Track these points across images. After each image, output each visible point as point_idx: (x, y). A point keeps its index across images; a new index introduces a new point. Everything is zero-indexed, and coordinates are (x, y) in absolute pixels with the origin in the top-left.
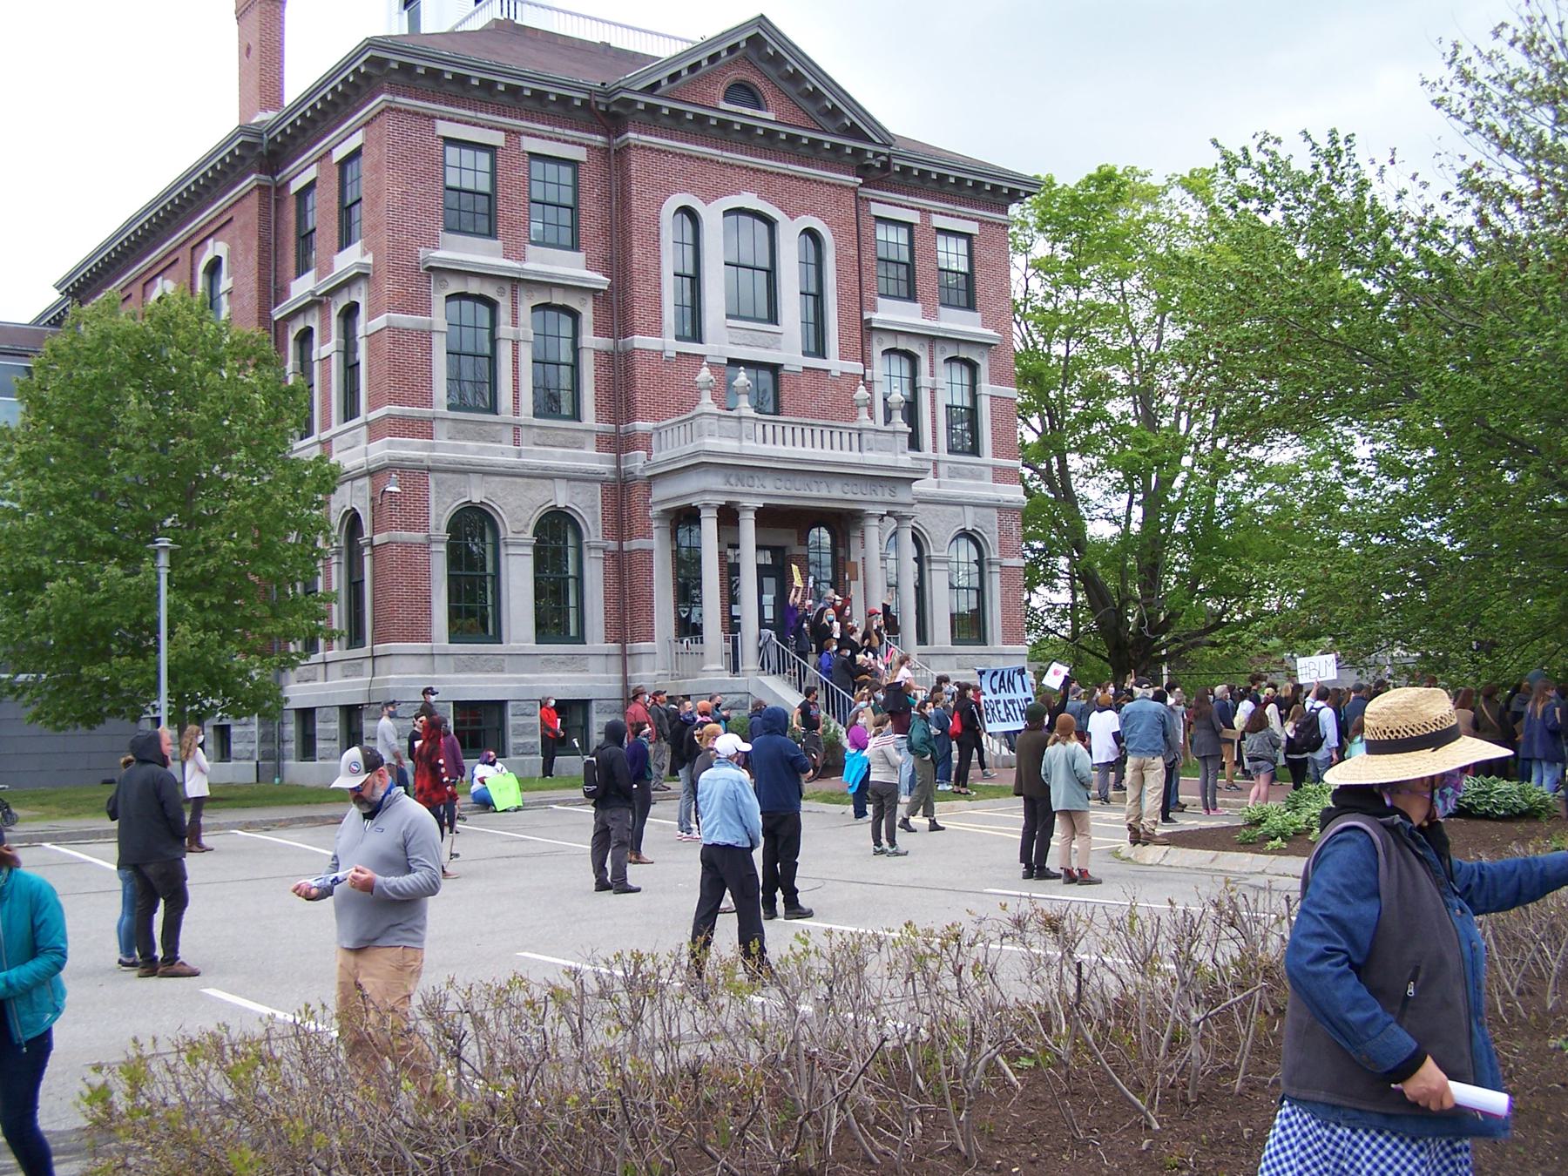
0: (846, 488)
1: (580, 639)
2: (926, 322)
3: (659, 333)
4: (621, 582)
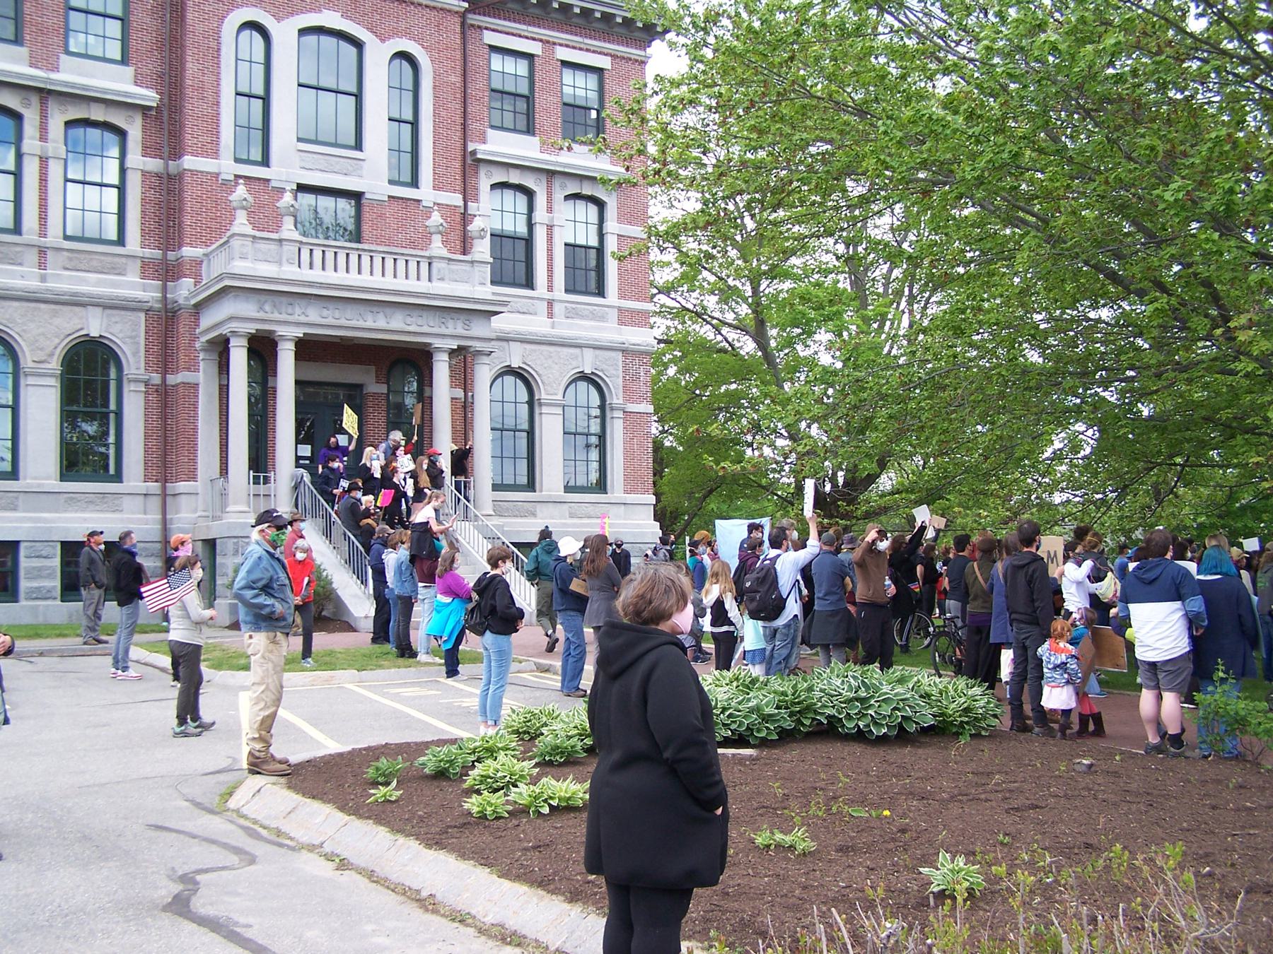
0: (409, 320)
1: (118, 478)
2: (545, 157)
3: (215, 154)
4: (164, 417)
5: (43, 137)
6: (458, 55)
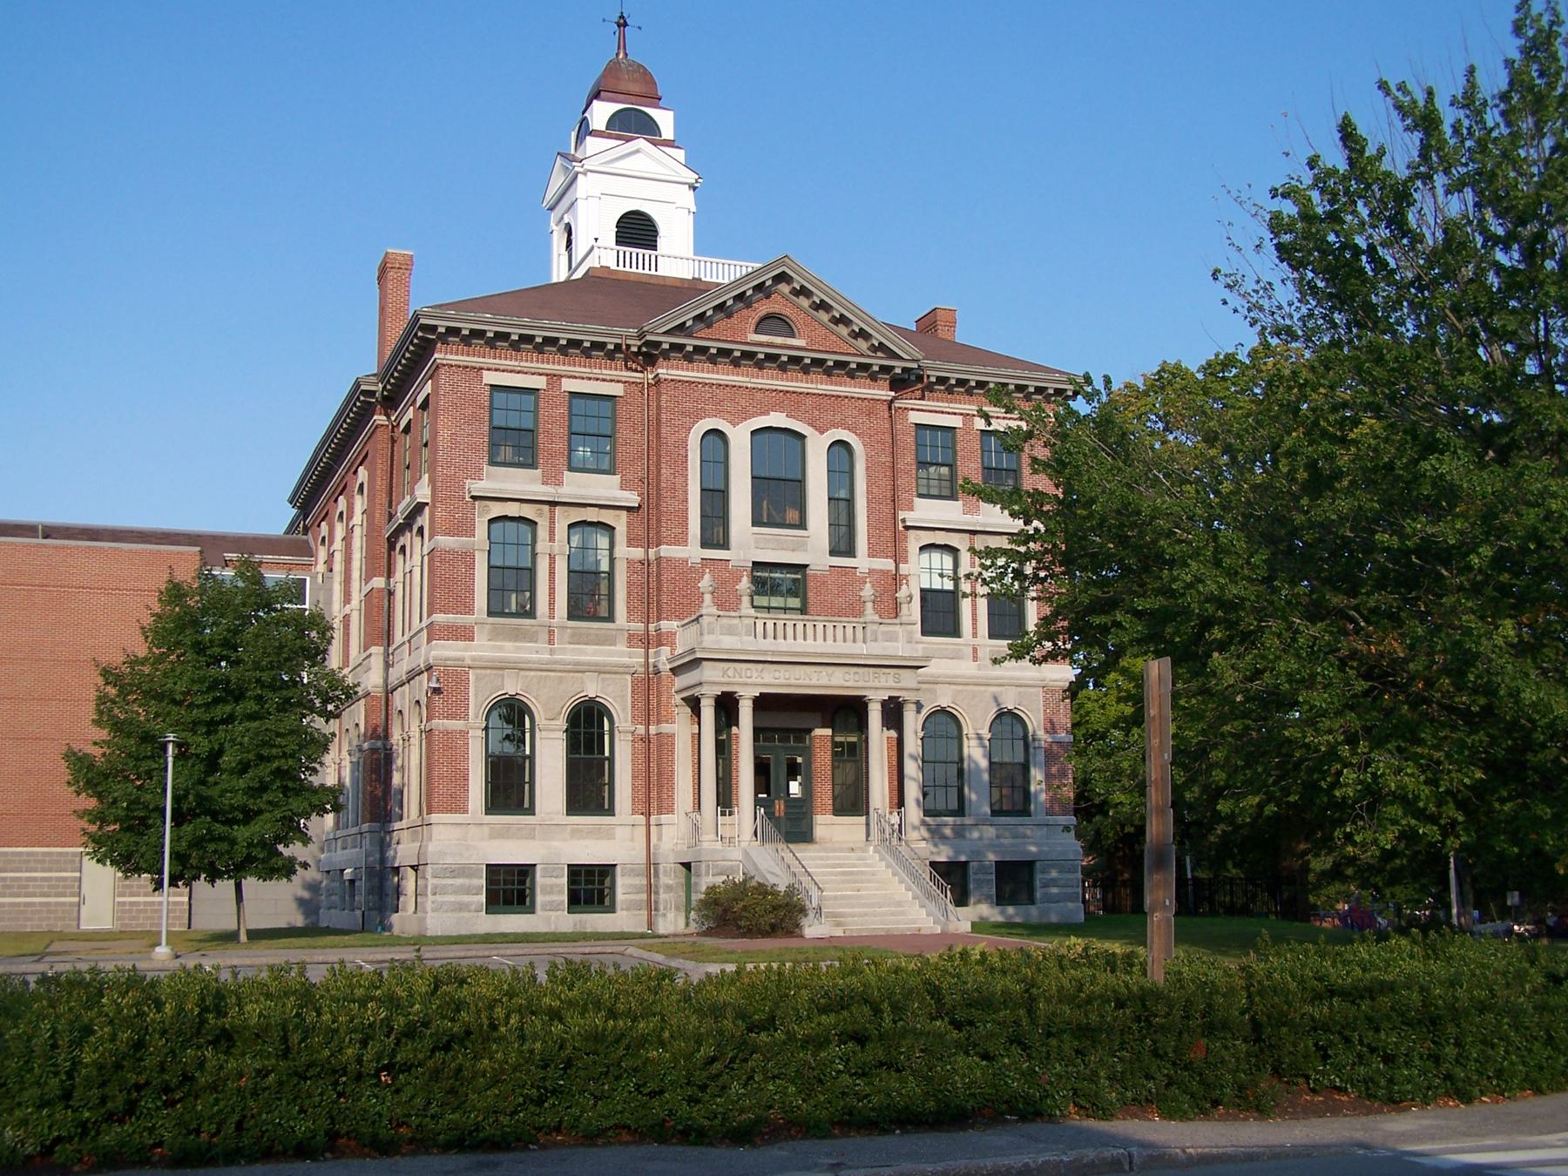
3: (685, 542)
5: (552, 539)
6: (888, 438)
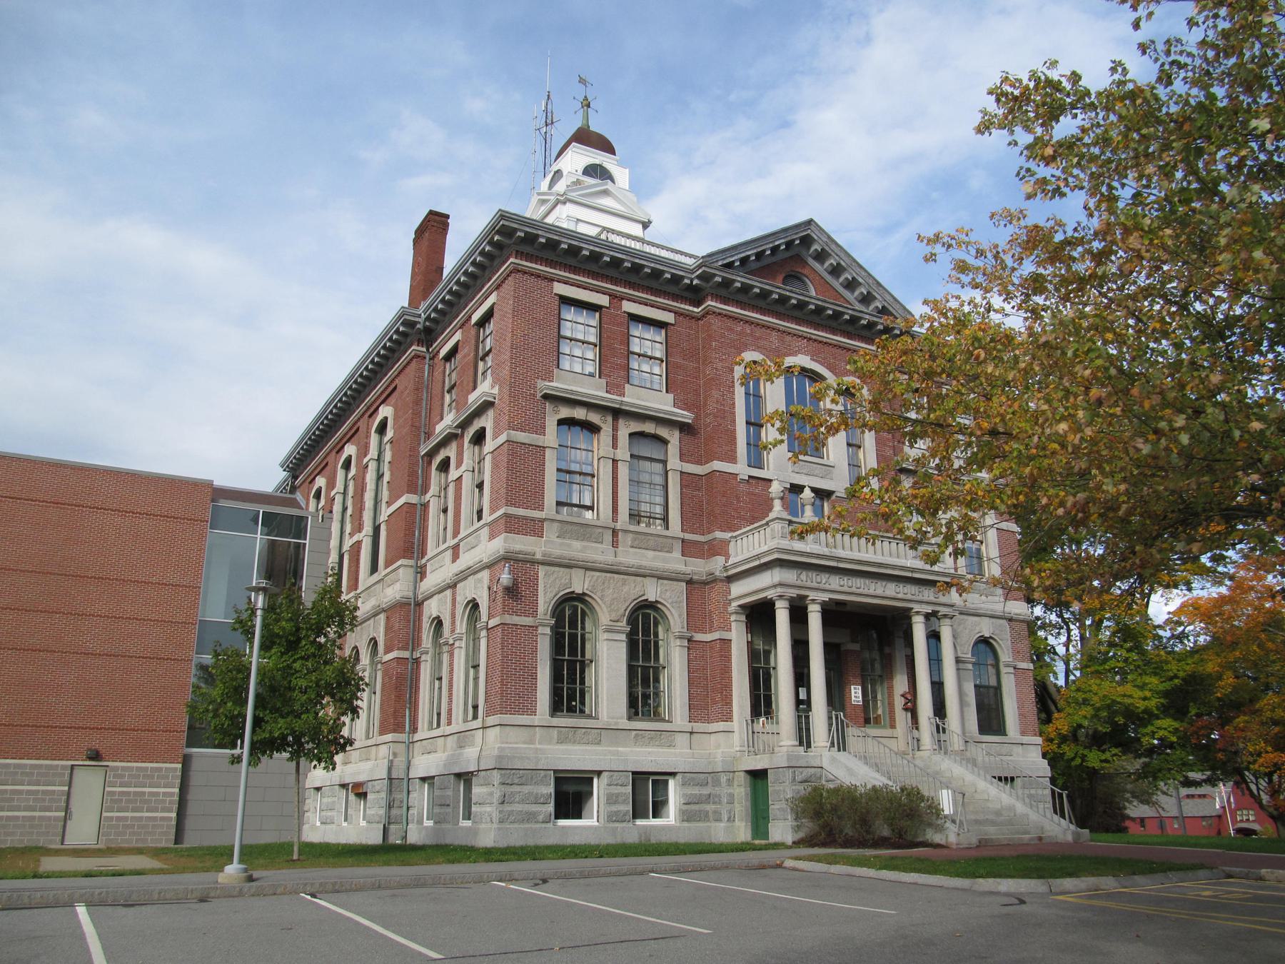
3: (732, 459)
